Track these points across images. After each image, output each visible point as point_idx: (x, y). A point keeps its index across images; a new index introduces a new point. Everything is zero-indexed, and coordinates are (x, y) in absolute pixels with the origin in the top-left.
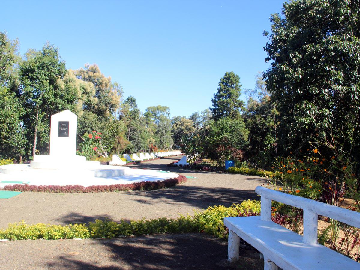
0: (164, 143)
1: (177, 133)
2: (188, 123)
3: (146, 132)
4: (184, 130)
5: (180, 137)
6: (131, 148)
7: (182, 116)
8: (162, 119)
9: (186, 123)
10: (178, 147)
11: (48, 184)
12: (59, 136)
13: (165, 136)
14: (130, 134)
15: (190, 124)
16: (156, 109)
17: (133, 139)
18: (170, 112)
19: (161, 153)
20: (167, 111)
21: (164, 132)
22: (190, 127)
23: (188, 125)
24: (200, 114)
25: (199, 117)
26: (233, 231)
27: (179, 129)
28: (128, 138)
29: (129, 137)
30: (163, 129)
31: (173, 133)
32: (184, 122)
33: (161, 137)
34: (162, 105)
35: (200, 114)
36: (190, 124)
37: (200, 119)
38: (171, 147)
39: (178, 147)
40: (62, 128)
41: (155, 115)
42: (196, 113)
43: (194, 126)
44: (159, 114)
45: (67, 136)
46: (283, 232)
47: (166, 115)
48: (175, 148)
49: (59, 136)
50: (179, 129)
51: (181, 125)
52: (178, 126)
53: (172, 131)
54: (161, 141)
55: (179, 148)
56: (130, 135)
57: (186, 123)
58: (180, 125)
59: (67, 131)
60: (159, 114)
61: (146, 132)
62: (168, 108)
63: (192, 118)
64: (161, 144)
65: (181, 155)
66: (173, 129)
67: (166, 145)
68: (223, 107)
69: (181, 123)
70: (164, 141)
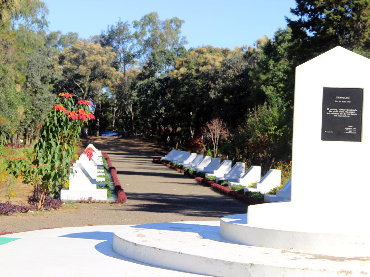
4: (85, 76)
7: (65, 32)
9: (92, 57)
11: (339, 256)
12: (326, 137)
15: (105, 59)
18: (48, 18)
20: (39, 17)
23: (98, 63)
24: (132, 30)
25: (129, 38)
32: (87, 53)
35: (132, 30)
36: (105, 59)
37: (133, 45)
40: (334, 112)
42: (120, 24)
43: (115, 65)
45: (357, 137)
46: (196, 210)
49: (326, 137)
52: (67, 64)
58: (70, 61)
59: (357, 121)
68: (340, 17)
69: (75, 56)
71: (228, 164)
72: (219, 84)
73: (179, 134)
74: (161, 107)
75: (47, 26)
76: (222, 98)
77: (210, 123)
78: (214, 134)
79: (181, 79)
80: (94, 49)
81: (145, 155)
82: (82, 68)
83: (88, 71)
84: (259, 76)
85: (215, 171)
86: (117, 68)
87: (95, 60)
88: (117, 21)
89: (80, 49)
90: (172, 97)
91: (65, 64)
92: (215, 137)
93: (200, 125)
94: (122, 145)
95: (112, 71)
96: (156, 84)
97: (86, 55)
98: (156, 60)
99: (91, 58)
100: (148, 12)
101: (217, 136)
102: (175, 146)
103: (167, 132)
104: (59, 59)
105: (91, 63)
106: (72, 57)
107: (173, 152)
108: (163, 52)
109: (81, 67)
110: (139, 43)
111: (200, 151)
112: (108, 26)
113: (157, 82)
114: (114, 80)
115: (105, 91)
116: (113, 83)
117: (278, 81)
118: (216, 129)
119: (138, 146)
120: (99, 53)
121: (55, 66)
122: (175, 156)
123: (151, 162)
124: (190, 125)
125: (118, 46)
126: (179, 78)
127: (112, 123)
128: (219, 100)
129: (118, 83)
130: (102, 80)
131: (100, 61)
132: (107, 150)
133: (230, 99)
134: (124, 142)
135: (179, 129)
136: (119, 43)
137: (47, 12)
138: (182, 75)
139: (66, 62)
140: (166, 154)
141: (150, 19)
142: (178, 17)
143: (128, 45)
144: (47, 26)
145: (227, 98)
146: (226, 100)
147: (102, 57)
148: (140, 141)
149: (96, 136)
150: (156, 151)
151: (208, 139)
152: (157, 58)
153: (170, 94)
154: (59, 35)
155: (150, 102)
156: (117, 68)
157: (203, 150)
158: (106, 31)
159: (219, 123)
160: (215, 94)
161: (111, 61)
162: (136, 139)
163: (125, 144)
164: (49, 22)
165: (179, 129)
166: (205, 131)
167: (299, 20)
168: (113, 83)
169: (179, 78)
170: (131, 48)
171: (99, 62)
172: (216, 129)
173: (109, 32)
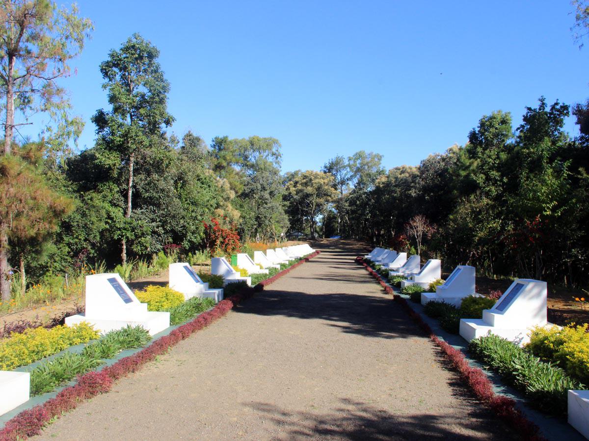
0: (267, 222)
3: (209, 186)
4: (312, 195)
6: (137, 237)
8: (262, 167)
9: (317, 181)
10: (296, 234)
13: (269, 205)
14: (133, 181)
16: (248, 143)
17: (150, 201)
18: (281, 151)
19: (577, 123)
20: (274, 150)
21: (266, 195)
22: (326, 187)
23: (321, 185)
24: (346, 162)
25: (344, 167)
26: (286, 254)
27: (300, 194)
30: (264, 189)
31: (287, 203)
32: (313, 178)
33: (258, 208)
34: (262, 135)
38: (282, 234)
39: (296, 234)
41: (246, 158)
43: (335, 186)
44: (253, 157)
47: (271, 159)
50: (300, 194)
51: (306, 184)
52: (299, 187)
53: (285, 198)
56: (134, 187)
57: (317, 181)
58: (302, 184)
61: (209, 186)
62: (276, 142)
63: (330, 169)
64: (260, 225)
66: (287, 194)
67: (272, 229)
71: (538, 295)
72: (419, 183)
73: (383, 236)
74: (368, 214)
75: (281, 157)
76: (423, 196)
77: (413, 220)
78: (417, 231)
79: (383, 187)
81: (355, 252)
84: (459, 173)
85: (497, 318)
86: (336, 189)
87: (318, 183)
88: (336, 156)
90: (375, 202)
92: (419, 234)
93: (401, 227)
94: (340, 244)
96: (363, 196)
97: (312, 179)
98: (363, 180)
100: (358, 151)
101: (420, 233)
102: (380, 244)
103: (373, 235)
104: (294, 184)
106: (303, 181)
107: (376, 250)
108: (369, 175)
110: (352, 171)
111: (404, 248)
113: (364, 194)
115: (330, 207)
116: (332, 198)
117: (489, 169)
118: (419, 226)
119: (352, 245)
120: (323, 178)
121: (291, 188)
122: (379, 256)
123: (354, 261)
124: (391, 227)
126: (381, 186)
127: (337, 230)
128: (420, 199)
130: (325, 197)
131: (323, 183)
133: (431, 197)
134: (343, 242)
135: (382, 232)
136: (337, 171)
137: (280, 146)
138: (383, 183)
139: (298, 185)
140: (370, 251)
141: (359, 156)
142: (379, 153)
143: (344, 172)
144: (281, 157)
145: (428, 196)
146: (426, 198)
147: (325, 181)
148: (354, 241)
149: (322, 238)
150: (365, 249)
151: (412, 236)
152: (364, 178)
153: (374, 199)
154: (300, 173)
155: (359, 210)
156: (336, 189)
157: (407, 247)
158: (328, 163)
159: (422, 219)
160: (415, 192)
161: (331, 184)
162: (352, 240)
163: (343, 243)
165: (382, 232)
166: (408, 228)
167: (471, 141)
168: (332, 198)
169: (381, 186)
170: (346, 175)
172: (419, 226)
173: (330, 163)
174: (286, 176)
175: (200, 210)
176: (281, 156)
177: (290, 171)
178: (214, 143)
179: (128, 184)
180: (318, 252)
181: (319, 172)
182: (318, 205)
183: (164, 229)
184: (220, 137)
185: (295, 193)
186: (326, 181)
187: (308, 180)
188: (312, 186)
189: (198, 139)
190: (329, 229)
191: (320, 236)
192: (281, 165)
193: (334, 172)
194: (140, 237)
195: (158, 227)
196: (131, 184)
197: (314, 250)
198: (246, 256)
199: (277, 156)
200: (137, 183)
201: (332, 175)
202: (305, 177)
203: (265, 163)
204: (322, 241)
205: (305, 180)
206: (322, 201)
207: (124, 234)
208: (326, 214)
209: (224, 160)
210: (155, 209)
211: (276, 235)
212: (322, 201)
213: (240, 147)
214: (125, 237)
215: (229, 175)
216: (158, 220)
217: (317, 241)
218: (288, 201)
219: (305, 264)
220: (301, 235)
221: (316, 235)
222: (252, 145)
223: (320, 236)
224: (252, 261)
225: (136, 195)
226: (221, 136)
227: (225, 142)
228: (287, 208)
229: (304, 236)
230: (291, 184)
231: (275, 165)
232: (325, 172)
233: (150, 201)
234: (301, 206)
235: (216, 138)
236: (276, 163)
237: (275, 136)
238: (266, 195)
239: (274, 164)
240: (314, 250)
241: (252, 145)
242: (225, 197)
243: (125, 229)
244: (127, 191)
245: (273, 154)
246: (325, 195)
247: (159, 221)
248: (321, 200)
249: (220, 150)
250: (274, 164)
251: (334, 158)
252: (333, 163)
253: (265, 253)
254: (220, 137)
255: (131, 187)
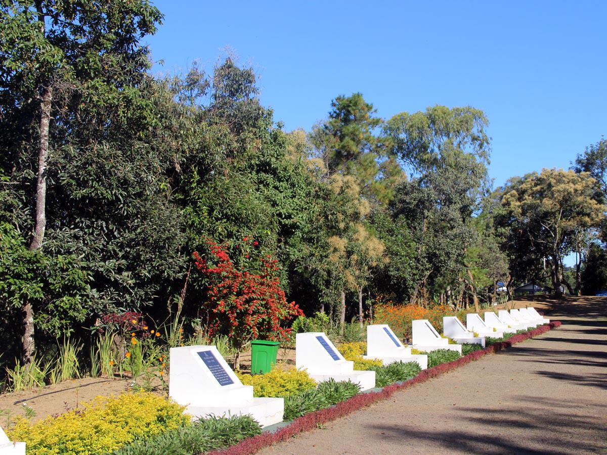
1: (525, 231)
2: (571, 185)
4: (554, 214)
5: (537, 245)
9: (561, 187)
10: (531, 287)
18: (489, 132)
20: (475, 131)
21: (454, 212)
22: (580, 199)
23: (569, 193)
28: (31, 203)
29: (42, 188)
31: (507, 231)
32: (553, 181)
39: (531, 287)
47: (468, 149)
48: (520, 295)
51: (541, 194)
52: (528, 200)
54: (431, 257)
55: (537, 293)
56: (51, 174)
57: (561, 187)
58: (533, 195)
60: (436, 145)
62: (477, 116)
65: (541, 329)
66: (505, 213)
70: (447, 254)
75: (488, 143)
80: (564, 177)
82: (547, 202)
83: (555, 205)
87: (564, 191)
89: (545, 177)
91: (526, 199)
95: (590, 204)
97: (552, 183)
99: (559, 187)
105: (559, 193)
106: (535, 189)
109: (545, 201)
112: (587, 148)
114: (594, 216)
116: (592, 219)
120: (574, 182)
121: (512, 203)
125: (602, 172)
129: (601, 220)
130: (578, 218)
131: (572, 191)
132: (585, 316)
137: (487, 123)
144: (488, 143)
158: (583, 155)
164: (491, 138)
168: (592, 219)
171: (571, 192)
174: (509, 184)
175: (248, 235)
176: (489, 141)
177: (517, 175)
178: (335, 109)
179: (36, 170)
180: (552, 326)
181: (565, 171)
182: (567, 233)
183: (136, 276)
184: (346, 97)
185: (520, 210)
186: (579, 187)
187: (543, 186)
188: (552, 197)
189: (248, 77)
190: (592, 277)
191: (573, 293)
192: (491, 159)
193: (596, 171)
194: (59, 296)
195: (119, 271)
196: (42, 169)
197: (546, 320)
198: (385, 329)
199: (480, 141)
200: (55, 164)
201: (592, 175)
202: (539, 181)
203: (457, 155)
204: (575, 300)
205: (538, 187)
206: (571, 224)
207: (13, 288)
208: (585, 252)
209: (353, 140)
210: (111, 227)
211: (475, 289)
212: (571, 224)
213: (412, 126)
214: (17, 296)
215: (365, 170)
216: (120, 254)
217: (566, 300)
218: (508, 226)
219: (503, 359)
220: (538, 290)
221: (564, 289)
222: (433, 122)
223: (573, 293)
224: (464, 328)
225: (57, 195)
226: (348, 95)
227: (356, 104)
228: (505, 240)
229: (545, 290)
230: (512, 196)
231: (478, 160)
232: (578, 171)
233: (94, 209)
234: (535, 236)
235: (338, 99)
236: (480, 156)
237: (477, 106)
238: (454, 212)
239: (477, 157)
240: (546, 320)
241: (433, 122)
242: (350, 211)
243: (18, 276)
244: (35, 182)
245: (474, 139)
246: (578, 214)
247: (124, 257)
248: (571, 223)
249: (346, 121)
250: (477, 157)
251: (595, 144)
252: (593, 153)
253: (497, 314)
254: (346, 97)
255: (43, 175)
